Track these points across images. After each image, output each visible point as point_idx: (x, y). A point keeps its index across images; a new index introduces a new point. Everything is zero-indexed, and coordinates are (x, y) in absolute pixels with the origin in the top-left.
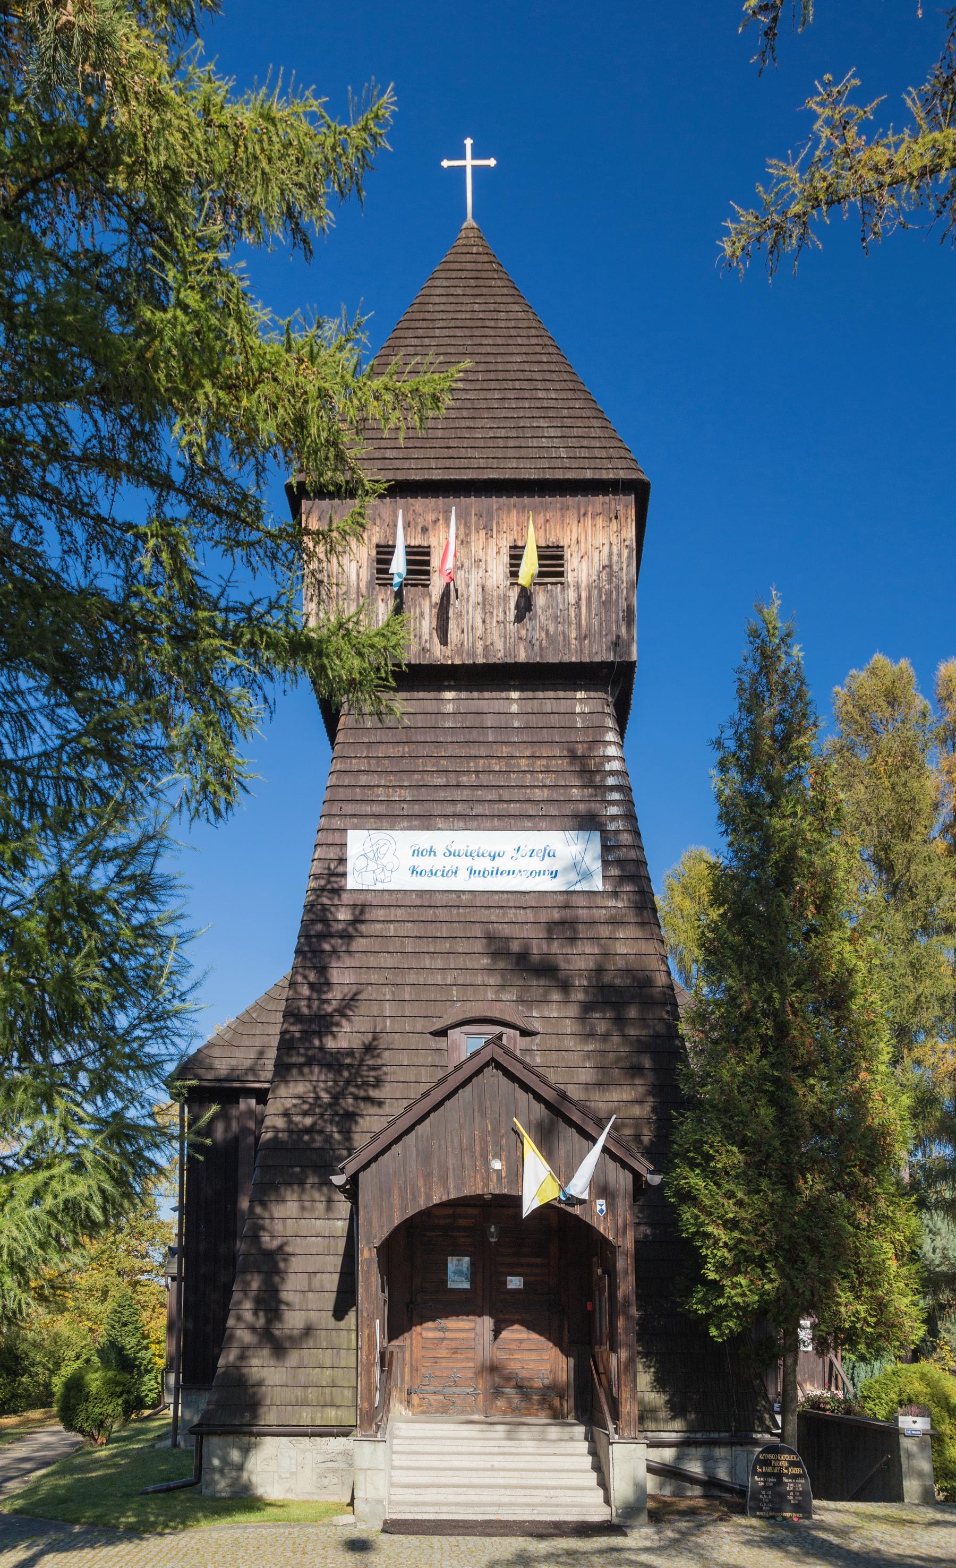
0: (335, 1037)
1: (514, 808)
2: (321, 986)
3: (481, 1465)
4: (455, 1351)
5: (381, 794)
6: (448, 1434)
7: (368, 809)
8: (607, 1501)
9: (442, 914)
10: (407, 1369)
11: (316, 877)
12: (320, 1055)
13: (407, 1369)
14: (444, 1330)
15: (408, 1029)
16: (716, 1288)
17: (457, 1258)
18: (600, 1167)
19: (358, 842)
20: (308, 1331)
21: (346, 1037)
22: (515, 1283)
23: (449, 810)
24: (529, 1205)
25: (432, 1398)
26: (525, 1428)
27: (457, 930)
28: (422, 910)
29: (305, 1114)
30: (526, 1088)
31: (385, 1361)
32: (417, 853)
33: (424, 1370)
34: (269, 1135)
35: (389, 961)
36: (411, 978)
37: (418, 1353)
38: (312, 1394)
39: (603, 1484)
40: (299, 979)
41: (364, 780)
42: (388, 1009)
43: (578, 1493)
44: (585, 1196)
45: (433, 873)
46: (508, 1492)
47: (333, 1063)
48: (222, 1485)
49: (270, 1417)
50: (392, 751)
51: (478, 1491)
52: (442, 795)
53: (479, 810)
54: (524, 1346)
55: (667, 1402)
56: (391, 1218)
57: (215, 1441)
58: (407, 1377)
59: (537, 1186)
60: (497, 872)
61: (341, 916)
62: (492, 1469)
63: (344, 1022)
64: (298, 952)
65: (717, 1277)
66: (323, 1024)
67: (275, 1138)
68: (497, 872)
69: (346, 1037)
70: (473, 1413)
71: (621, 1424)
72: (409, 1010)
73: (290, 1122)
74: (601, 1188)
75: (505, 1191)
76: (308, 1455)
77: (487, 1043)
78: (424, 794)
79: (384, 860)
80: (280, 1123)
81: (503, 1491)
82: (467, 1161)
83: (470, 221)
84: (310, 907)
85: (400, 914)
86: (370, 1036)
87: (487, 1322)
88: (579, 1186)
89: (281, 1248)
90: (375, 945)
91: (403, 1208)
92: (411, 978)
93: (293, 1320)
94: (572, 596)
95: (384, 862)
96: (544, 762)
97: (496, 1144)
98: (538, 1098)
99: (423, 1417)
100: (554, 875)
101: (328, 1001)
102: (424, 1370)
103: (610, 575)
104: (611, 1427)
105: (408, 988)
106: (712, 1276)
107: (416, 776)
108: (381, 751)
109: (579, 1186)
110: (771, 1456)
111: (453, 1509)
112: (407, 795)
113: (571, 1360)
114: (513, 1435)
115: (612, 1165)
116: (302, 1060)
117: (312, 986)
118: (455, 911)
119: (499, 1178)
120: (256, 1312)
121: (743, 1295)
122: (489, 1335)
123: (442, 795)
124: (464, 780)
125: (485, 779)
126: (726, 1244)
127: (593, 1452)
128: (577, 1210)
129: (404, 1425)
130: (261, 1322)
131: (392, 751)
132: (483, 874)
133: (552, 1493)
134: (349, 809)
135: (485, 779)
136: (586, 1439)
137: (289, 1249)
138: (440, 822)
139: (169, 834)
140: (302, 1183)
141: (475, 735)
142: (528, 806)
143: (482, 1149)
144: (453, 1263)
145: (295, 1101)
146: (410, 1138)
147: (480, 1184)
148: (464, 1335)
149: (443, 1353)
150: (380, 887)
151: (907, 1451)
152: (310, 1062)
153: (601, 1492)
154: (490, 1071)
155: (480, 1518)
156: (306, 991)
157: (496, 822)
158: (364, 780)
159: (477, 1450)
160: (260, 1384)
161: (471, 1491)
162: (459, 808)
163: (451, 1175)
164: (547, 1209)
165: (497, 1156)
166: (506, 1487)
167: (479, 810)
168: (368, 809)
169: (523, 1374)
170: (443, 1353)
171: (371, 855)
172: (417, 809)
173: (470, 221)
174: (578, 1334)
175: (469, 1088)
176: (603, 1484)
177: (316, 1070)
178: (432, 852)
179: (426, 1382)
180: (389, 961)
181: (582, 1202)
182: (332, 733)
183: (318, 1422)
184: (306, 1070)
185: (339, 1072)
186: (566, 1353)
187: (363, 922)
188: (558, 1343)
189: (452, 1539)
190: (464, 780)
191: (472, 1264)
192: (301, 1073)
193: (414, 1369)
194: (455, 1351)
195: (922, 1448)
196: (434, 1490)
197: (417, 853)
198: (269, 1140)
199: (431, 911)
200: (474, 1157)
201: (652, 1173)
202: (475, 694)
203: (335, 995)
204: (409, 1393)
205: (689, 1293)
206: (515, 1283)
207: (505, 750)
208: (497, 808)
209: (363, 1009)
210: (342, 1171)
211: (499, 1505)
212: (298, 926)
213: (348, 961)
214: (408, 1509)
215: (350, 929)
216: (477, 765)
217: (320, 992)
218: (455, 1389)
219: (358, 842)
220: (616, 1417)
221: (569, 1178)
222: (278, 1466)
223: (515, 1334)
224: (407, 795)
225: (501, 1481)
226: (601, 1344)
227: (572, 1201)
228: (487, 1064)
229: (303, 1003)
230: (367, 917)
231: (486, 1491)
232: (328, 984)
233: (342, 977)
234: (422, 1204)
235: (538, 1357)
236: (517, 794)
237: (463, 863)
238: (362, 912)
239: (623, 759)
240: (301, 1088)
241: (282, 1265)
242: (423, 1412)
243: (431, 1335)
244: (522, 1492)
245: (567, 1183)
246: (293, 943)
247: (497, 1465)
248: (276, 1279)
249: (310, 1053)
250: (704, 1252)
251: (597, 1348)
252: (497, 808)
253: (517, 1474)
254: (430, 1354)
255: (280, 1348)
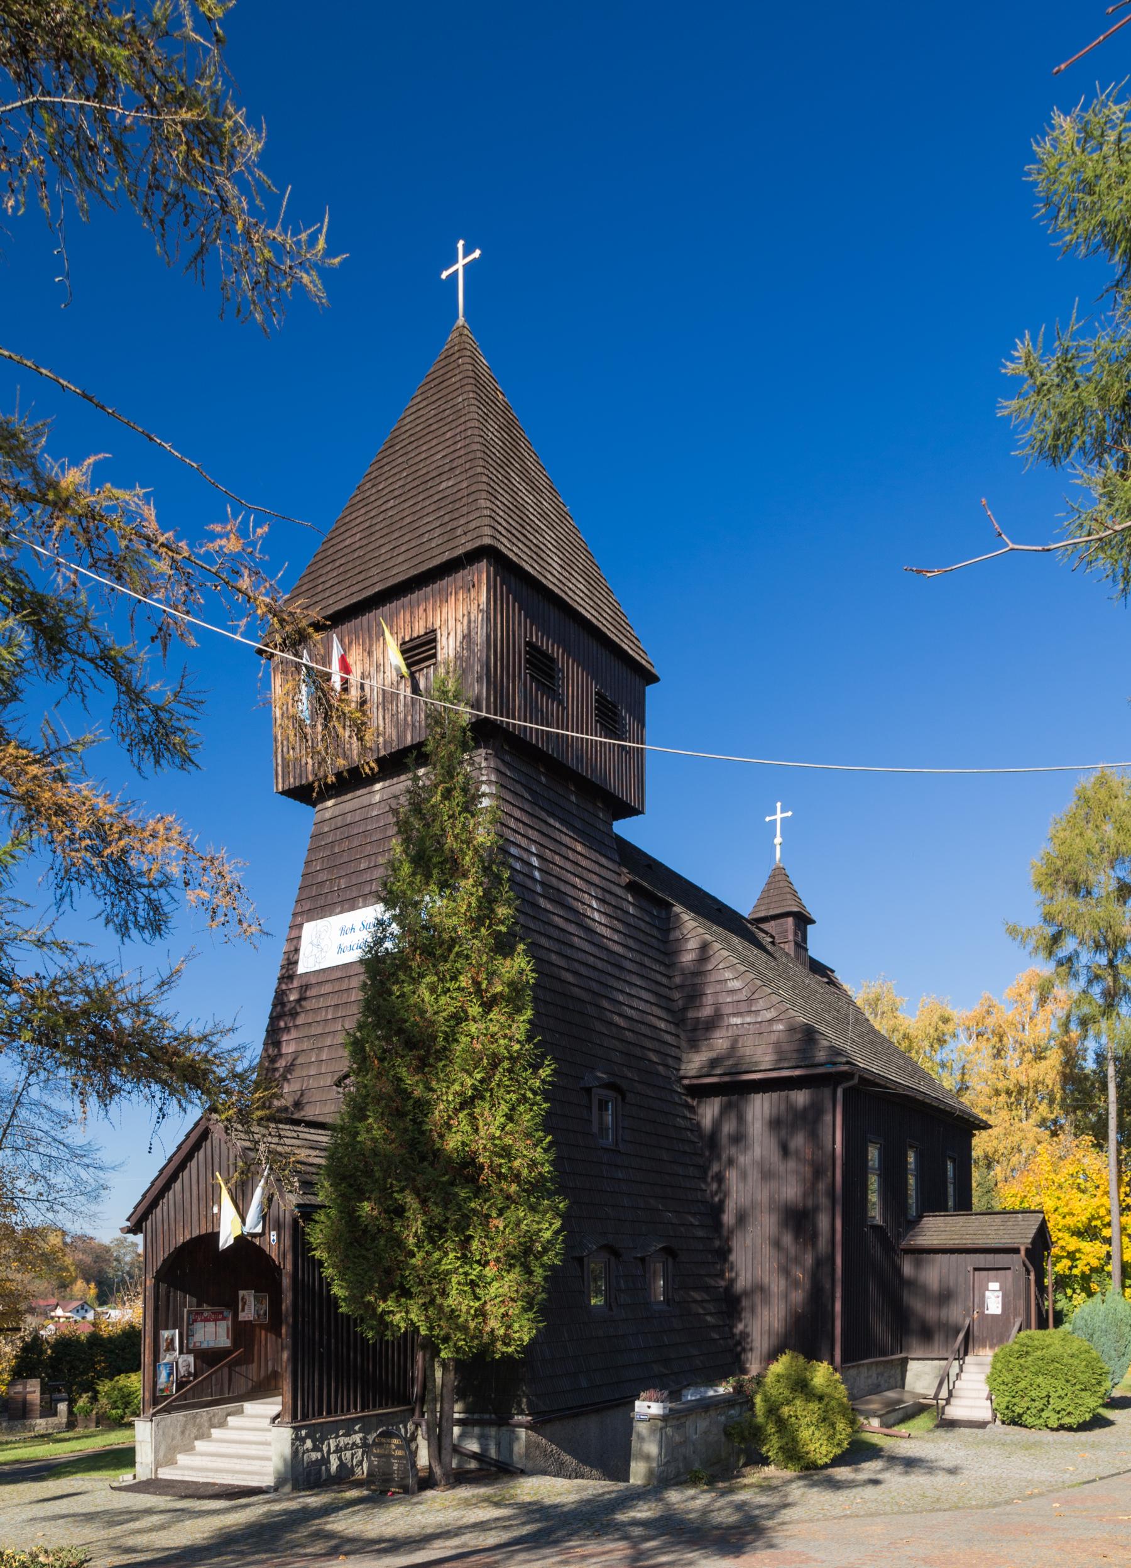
83: (461, 321)
94: (442, 670)
103: (469, 643)
110: (383, 1440)
139: (374, 921)
151: (639, 1435)
164: (240, 1240)
173: (461, 321)
187: (305, 999)
195: (653, 1431)
197: (344, 931)
202: (395, 780)
213: (294, 1034)
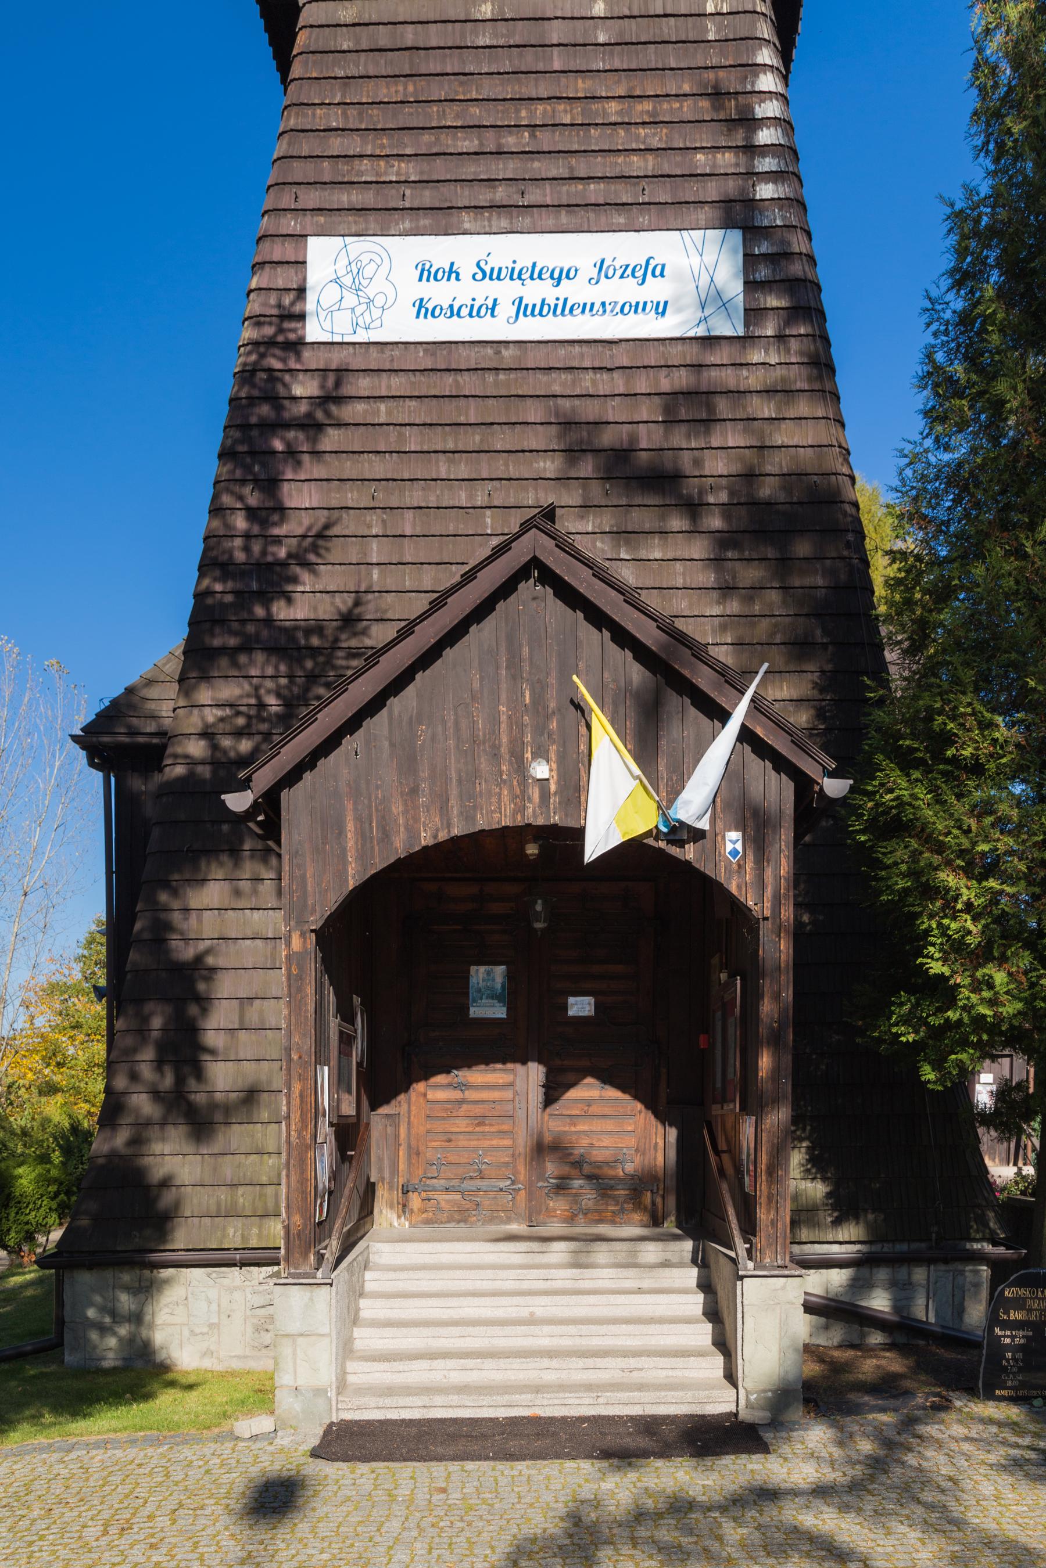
0: (289, 601)
1: (595, 192)
2: (269, 512)
3: (512, 1313)
4: (481, 1121)
5: (366, 170)
6: (462, 1259)
7: (344, 198)
8: (731, 1377)
9: (469, 384)
10: (402, 1153)
11: (258, 320)
12: (265, 633)
13: (402, 1153)
14: (462, 1086)
15: (408, 585)
16: (942, 992)
17: (480, 958)
18: (731, 772)
19: (325, 257)
20: (251, 1096)
21: (307, 603)
22: (580, 1006)
23: (484, 196)
24: (596, 845)
25: (443, 1198)
26: (603, 1246)
27: (495, 411)
28: (435, 377)
29: (239, 734)
30: (597, 618)
31: (349, 1137)
32: (426, 273)
33: (429, 1154)
34: (179, 770)
35: (378, 468)
36: (415, 496)
37: (420, 1127)
38: (244, 1198)
39: (724, 1345)
40: (227, 500)
41: (336, 145)
42: (375, 552)
43: (680, 1362)
44: (704, 824)
45: (454, 312)
46: (555, 1363)
47: (285, 644)
48: (109, 1348)
49: (182, 1237)
50: (384, 91)
51: (503, 1363)
52: (470, 169)
53: (534, 195)
54: (595, 1109)
55: (829, 1195)
56: (342, 875)
57: (85, 1278)
58: (402, 1166)
59: (614, 808)
60: (564, 308)
61: (298, 391)
62: (531, 1321)
63: (305, 576)
64: (225, 455)
65: (946, 971)
66: (272, 579)
67: (191, 775)
68: (564, 308)
69: (307, 603)
70: (509, 1220)
71: (760, 1241)
72: (410, 552)
73: (215, 747)
74: (736, 803)
75: (556, 819)
76: (237, 1295)
77: (526, 527)
78: (440, 169)
79: (372, 289)
80: (196, 748)
81: (546, 1362)
82: (484, 765)
84: (246, 375)
85: (397, 384)
86: (350, 599)
87: (534, 1073)
88: (693, 804)
89: (199, 959)
90: (353, 440)
91: (362, 857)
92: (415, 496)
93: (222, 1078)
95: (371, 292)
96: (648, 106)
97: (540, 729)
98: (622, 637)
99: (427, 1230)
100: (661, 309)
101: (278, 540)
102: (429, 1154)
104: (741, 1247)
105: (409, 515)
106: (937, 968)
107: (427, 137)
108: (365, 92)
109: (693, 804)
111: (454, 1399)
112: (411, 170)
113: (673, 1133)
114: (583, 1259)
115: (758, 768)
116: (233, 642)
117: (252, 513)
118: (490, 377)
119: (545, 795)
120: (159, 1064)
121: (993, 1003)
122: (536, 1095)
123: (470, 169)
124: (510, 141)
125: (546, 140)
126: (969, 906)
127: (706, 1286)
128: (689, 853)
129: (393, 1248)
130: (168, 1081)
131: (384, 91)
132: (541, 310)
133: (633, 1362)
134: (311, 198)
135: (546, 140)
136: (694, 1261)
137: (210, 961)
138: (467, 220)
140: (235, 853)
141: (529, 60)
142: (619, 186)
143: (512, 741)
144: (478, 974)
145: (219, 713)
146: (378, 724)
147: (508, 808)
148: (496, 1095)
149: (461, 1125)
150: (362, 337)
152: (246, 648)
153: (719, 1360)
154: (528, 589)
155: (501, 1413)
156: (240, 523)
157: (564, 218)
158: (336, 145)
159: (510, 1285)
160: (166, 1183)
161: (489, 1363)
162: (501, 194)
163: (454, 792)
164: (632, 854)
165: (541, 753)
166: (551, 1354)
167: (534, 195)
168: (344, 198)
169: (598, 1155)
170: (461, 1125)
171: (347, 281)
172: (427, 197)
174: (683, 1089)
175: (490, 623)
176: (724, 1345)
177: (260, 657)
178: (453, 273)
179: (433, 1171)
180: (378, 468)
181: (697, 835)
182: (284, 61)
183: (254, 1243)
184: (243, 659)
185: (300, 661)
186: (663, 1117)
188: (651, 1104)
189: (438, 1469)
190: (510, 141)
191: (510, 976)
192: (235, 664)
193: (414, 1153)
194: (481, 1121)
196: (424, 1364)
197: (426, 273)
198: (179, 780)
199: (449, 379)
200: (496, 756)
201: (832, 775)
203: (292, 527)
204: (405, 1192)
205: (881, 1009)
206: (580, 1006)
207: (582, 86)
208: (569, 192)
209: (337, 551)
210: (245, 785)
211: (538, 1389)
212: (224, 410)
213: (312, 469)
214: (372, 1401)
215: (320, 415)
216: (532, 113)
217: (264, 523)
218: (479, 1183)
219: (325, 257)
220: (749, 1229)
221: (675, 791)
222: (196, 1316)
223: (589, 1091)
224: (411, 170)
225: (545, 1342)
226: (724, 1100)
227: (681, 833)
228: (521, 574)
229: (238, 542)
230: (347, 390)
231: (516, 1363)
232: (281, 510)
233: (303, 496)
234: (400, 847)
235: (619, 1127)
236: (600, 166)
237: (506, 291)
238: (338, 384)
239: (784, 98)
240: (230, 690)
241: (201, 987)
242: (428, 1222)
243: (441, 1095)
244: (580, 1363)
245: (669, 808)
246: (216, 439)
247: (540, 1312)
248: (193, 1010)
249: (251, 628)
250: (925, 923)
251: (716, 1110)
252: (569, 192)
253: (572, 1329)
254: (439, 1126)
255: (201, 1122)
